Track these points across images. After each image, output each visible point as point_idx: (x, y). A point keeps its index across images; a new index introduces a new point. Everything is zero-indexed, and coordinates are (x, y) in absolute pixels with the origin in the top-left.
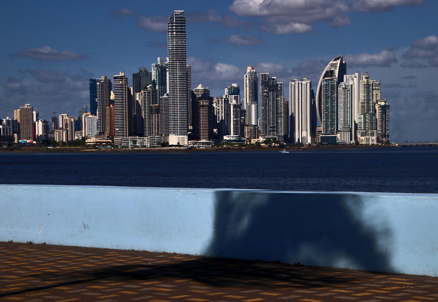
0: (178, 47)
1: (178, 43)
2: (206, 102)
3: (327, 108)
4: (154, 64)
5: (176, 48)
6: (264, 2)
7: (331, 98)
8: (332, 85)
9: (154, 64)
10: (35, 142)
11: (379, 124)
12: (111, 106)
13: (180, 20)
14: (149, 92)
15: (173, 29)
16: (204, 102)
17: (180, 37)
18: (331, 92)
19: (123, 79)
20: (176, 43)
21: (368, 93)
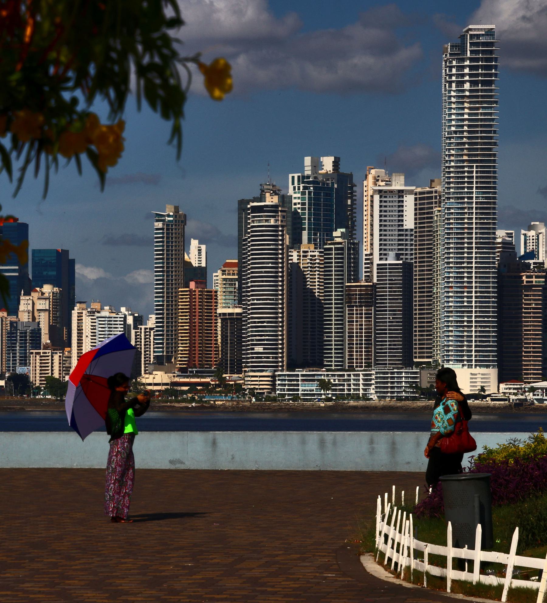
0: (477, 126)
1: (477, 114)
2: (537, 277)
4: (296, 176)
5: (469, 126)
6: (527, 4)
9: (296, 176)
12: (192, 285)
13: (483, 52)
14: (342, 249)
15: (463, 75)
16: (531, 277)
17: (482, 96)
19: (277, 212)
20: (469, 114)
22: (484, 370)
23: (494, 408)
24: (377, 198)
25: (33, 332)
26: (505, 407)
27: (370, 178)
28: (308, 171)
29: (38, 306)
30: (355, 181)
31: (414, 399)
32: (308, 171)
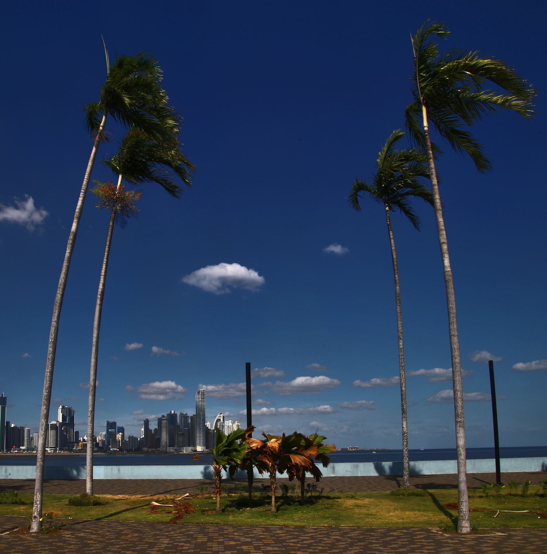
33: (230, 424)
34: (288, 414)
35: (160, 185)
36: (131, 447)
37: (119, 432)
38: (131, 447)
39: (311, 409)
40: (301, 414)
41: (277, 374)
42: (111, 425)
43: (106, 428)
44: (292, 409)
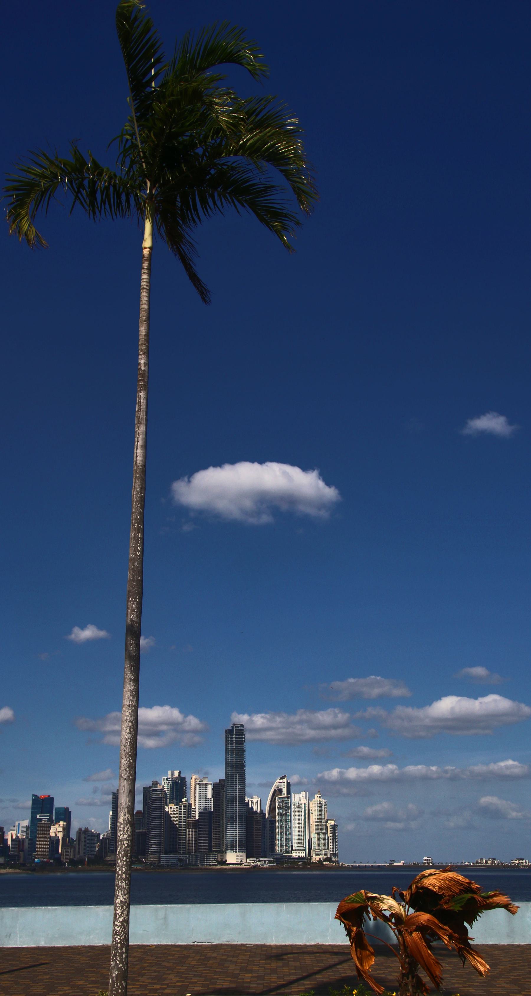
3: (281, 826)
7: (286, 817)
8: (286, 803)
10: (51, 861)
11: (331, 843)
18: (286, 810)
21: (321, 811)
22: (241, 854)
23: (246, 869)
24: (198, 786)
25: (56, 840)
26: (250, 868)
27: (193, 779)
28: (169, 776)
29: (58, 830)
30: (186, 780)
31: (215, 865)
32: (169, 776)
33: (304, 801)
34: (425, 778)
35: (181, 266)
36: (82, 854)
37: (58, 821)
38: (82, 854)
39: (480, 768)
40: (454, 778)
41: (398, 692)
42: (42, 805)
43: (29, 813)
44: (434, 768)
